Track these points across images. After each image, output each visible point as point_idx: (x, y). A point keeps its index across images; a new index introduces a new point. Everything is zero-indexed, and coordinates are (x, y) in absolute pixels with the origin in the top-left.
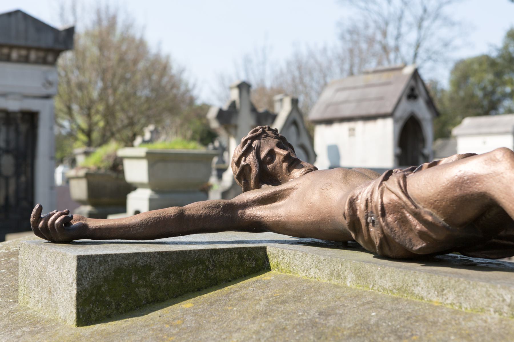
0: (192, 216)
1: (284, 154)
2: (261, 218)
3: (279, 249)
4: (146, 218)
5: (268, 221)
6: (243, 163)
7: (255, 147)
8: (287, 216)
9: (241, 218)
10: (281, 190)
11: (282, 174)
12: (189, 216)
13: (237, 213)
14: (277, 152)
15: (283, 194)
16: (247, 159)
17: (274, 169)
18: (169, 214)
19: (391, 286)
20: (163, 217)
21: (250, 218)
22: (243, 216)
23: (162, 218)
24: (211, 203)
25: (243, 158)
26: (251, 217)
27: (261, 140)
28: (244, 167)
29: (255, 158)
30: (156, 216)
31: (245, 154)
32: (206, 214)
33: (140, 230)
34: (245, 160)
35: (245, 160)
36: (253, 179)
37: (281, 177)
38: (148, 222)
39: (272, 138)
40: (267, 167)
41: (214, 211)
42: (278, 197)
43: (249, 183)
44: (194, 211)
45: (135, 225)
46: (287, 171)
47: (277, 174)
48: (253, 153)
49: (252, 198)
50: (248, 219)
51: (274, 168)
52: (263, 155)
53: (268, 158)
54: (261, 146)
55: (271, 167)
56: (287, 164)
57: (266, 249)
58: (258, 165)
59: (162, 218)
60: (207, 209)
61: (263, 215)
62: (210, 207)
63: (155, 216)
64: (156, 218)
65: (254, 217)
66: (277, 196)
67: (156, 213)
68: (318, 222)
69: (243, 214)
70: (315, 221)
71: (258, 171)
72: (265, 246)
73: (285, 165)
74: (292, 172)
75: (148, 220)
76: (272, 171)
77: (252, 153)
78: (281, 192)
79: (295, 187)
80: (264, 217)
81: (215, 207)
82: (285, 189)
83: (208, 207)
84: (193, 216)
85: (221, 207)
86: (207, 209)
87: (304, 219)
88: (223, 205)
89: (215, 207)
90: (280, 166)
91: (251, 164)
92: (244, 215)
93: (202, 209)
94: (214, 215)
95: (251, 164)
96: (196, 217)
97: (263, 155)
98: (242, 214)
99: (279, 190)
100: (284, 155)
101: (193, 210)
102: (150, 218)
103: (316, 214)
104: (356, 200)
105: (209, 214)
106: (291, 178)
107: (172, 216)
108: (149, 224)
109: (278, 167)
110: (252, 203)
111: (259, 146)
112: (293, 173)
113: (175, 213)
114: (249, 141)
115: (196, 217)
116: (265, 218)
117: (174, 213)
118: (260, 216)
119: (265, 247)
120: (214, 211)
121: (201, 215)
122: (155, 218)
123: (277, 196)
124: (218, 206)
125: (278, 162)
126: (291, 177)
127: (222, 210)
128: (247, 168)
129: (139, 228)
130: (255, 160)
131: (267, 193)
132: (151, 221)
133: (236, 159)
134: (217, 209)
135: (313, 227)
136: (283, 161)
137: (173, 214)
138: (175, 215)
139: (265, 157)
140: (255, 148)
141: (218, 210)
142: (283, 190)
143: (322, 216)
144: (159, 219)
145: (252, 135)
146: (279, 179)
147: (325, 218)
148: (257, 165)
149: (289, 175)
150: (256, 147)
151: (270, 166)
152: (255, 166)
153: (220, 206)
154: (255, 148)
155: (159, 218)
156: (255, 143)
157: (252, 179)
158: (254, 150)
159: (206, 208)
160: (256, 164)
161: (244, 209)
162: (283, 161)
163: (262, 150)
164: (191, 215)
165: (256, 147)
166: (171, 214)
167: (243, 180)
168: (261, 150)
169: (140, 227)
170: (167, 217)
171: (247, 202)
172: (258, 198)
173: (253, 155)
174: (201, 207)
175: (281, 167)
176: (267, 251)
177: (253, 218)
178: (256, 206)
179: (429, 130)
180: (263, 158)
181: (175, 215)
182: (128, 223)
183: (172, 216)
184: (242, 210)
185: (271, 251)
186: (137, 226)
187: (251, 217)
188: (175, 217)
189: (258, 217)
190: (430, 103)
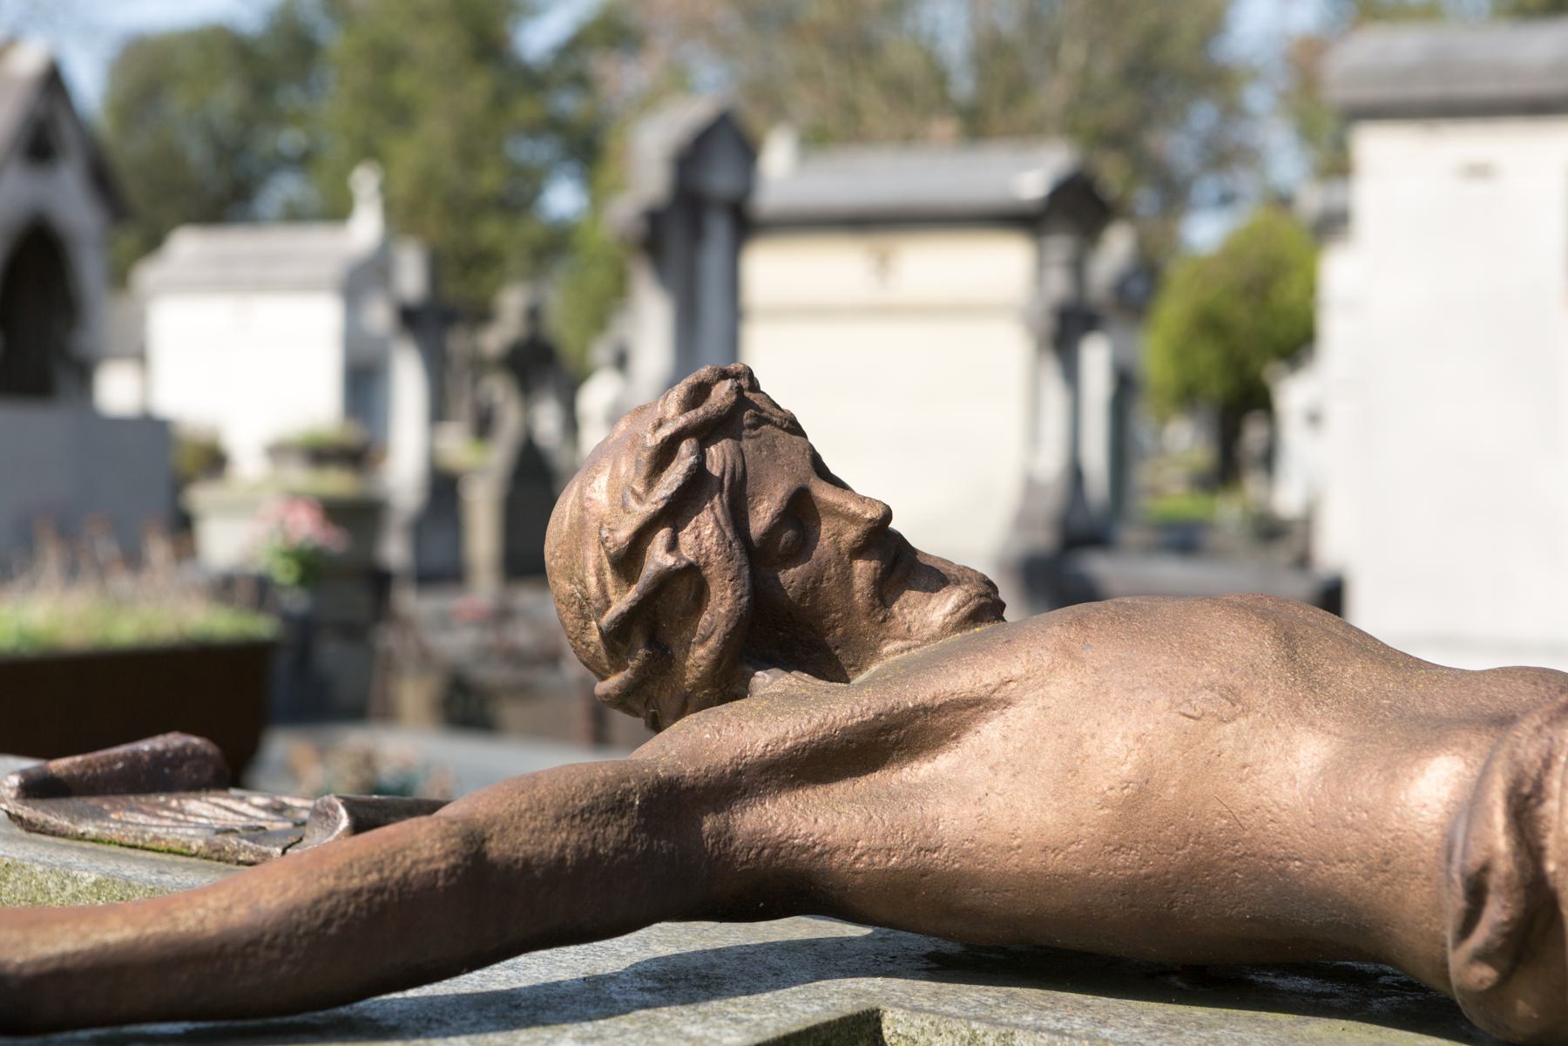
0: (520, 866)
1: (868, 516)
2: (821, 854)
3: (975, 1025)
4: (315, 895)
5: (857, 873)
6: (658, 557)
7: (723, 474)
8: (967, 845)
9: (720, 855)
10: (916, 710)
11: (848, 615)
12: (509, 867)
13: (701, 833)
14: (827, 504)
15: (922, 728)
16: (686, 538)
17: (814, 589)
18: (422, 868)
19: (327, 877)
20: (397, 883)
21: (759, 854)
22: (725, 844)
23: (391, 893)
24: (589, 785)
25: (662, 536)
26: (764, 848)
27: (740, 439)
28: (666, 580)
29: (729, 534)
30: (365, 884)
31: (675, 513)
32: (579, 849)
33: (284, 969)
34: (673, 546)
35: (673, 546)
36: (712, 643)
37: (839, 631)
38: (328, 923)
39: (781, 427)
40: (777, 579)
41: (612, 831)
42: (897, 742)
43: (672, 657)
44: (524, 836)
45: (255, 942)
46: (877, 602)
47: (823, 617)
48: (718, 510)
49: (760, 750)
50: (747, 862)
51: (813, 587)
52: (762, 516)
53: (788, 535)
54: (750, 470)
55: (798, 579)
56: (873, 564)
57: (878, 1020)
58: (746, 572)
59: (391, 893)
60: (578, 820)
61: (830, 838)
62: (591, 809)
63: (356, 883)
64: (365, 896)
65: (778, 847)
66: (892, 737)
67: (356, 866)
68: (1167, 882)
69: (724, 837)
70: (1148, 877)
71: (745, 599)
72: (864, 1004)
73: (863, 570)
74: (896, 608)
75: (326, 906)
76: (801, 600)
77: (712, 508)
78: (911, 721)
79: (997, 695)
80: (838, 848)
81: (612, 810)
82: (937, 703)
83: (583, 811)
84: (527, 862)
85: (633, 804)
86: (578, 820)
87: (1085, 865)
88: (642, 794)
89: (612, 810)
90: (843, 573)
91: (707, 564)
92: (731, 839)
93: (558, 820)
94: (617, 850)
95: (707, 564)
96: (538, 873)
97: (762, 516)
98: (719, 834)
99: (907, 709)
100: (871, 520)
101: (517, 828)
102: (335, 899)
103: (1158, 841)
104: (1533, 801)
105: (594, 851)
106: (895, 638)
107: (441, 874)
108: (333, 930)
109: (829, 579)
110: (762, 773)
111: (739, 470)
112: (901, 609)
113: (452, 860)
114: (686, 448)
115: (538, 873)
116: (839, 858)
117: (446, 856)
118: (815, 845)
119: (873, 1012)
120: (612, 831)
121: (561, 860)
122: (357, 893)
123: (892, 737)
124: (621, 801)
125: (831, 553)
126: (892, 633)
127: (643, 820)
128: (683, 591)
129: (275, 954)
130: (730, 546)
131: (843, 723)
132: (344, 915)
133: (624, 534)
134: (622, 817)
135: (1131, 906)
136: (858, 552)
137: (443, 866)
138: (451, 872)
139: (772, 532)
140: (726, 483)
141: (625, 821)
142: (926, 709)
143: (1193, 855)
144: (378, 899)
145: (692, 414)
146: (829, 639)
147: (1211, 865)
148: (740, 568)
149: (884, 620)
150: (727, 477)
151: (791, 577)
152: (729, 575)
153: (632, 797)
154: (726, 483)
155: (378, 890)
156: (718, 456)
157: (705, 639)
158: (721, 491)
159: (574, 817)
160: (735, 564)
161: (723, 810)
162: (858, 552)
163: (754, 495)
164: (516, 861)
165: (727, 477)
166: (433, 866)
167: (641, 644)
168: (748, 492)
169: (287, 949)
170: (415, 886)
171: (737, 773)
172: (794, 748)
173: (717, 521)
174: (550, 813)
175: (846, 578)
176: (886, 1033)
177: (775, 855)
178: (780, 788)
179: (90, 267)
180: (764, 534)
181: (455, 867)
182: (212, 927)
183: (441, 874)
184: (717, 813)
185: (913, 1032)
186: (270, 947)
187: (764, 848)
188: (454, 880)
189: (805, 849)
190: (102, 179)
